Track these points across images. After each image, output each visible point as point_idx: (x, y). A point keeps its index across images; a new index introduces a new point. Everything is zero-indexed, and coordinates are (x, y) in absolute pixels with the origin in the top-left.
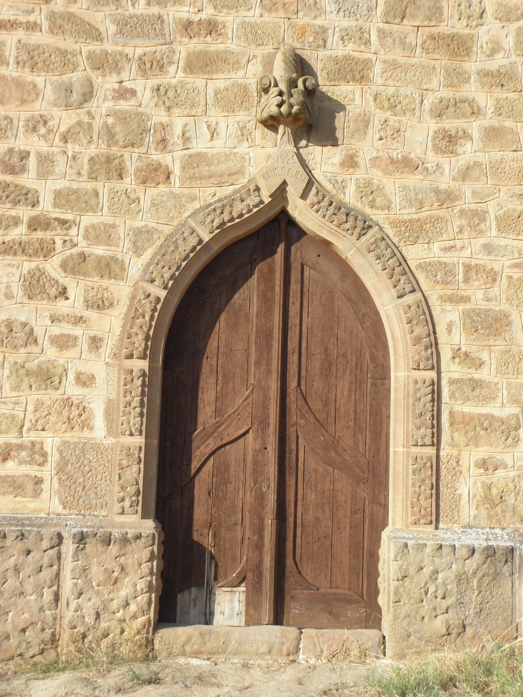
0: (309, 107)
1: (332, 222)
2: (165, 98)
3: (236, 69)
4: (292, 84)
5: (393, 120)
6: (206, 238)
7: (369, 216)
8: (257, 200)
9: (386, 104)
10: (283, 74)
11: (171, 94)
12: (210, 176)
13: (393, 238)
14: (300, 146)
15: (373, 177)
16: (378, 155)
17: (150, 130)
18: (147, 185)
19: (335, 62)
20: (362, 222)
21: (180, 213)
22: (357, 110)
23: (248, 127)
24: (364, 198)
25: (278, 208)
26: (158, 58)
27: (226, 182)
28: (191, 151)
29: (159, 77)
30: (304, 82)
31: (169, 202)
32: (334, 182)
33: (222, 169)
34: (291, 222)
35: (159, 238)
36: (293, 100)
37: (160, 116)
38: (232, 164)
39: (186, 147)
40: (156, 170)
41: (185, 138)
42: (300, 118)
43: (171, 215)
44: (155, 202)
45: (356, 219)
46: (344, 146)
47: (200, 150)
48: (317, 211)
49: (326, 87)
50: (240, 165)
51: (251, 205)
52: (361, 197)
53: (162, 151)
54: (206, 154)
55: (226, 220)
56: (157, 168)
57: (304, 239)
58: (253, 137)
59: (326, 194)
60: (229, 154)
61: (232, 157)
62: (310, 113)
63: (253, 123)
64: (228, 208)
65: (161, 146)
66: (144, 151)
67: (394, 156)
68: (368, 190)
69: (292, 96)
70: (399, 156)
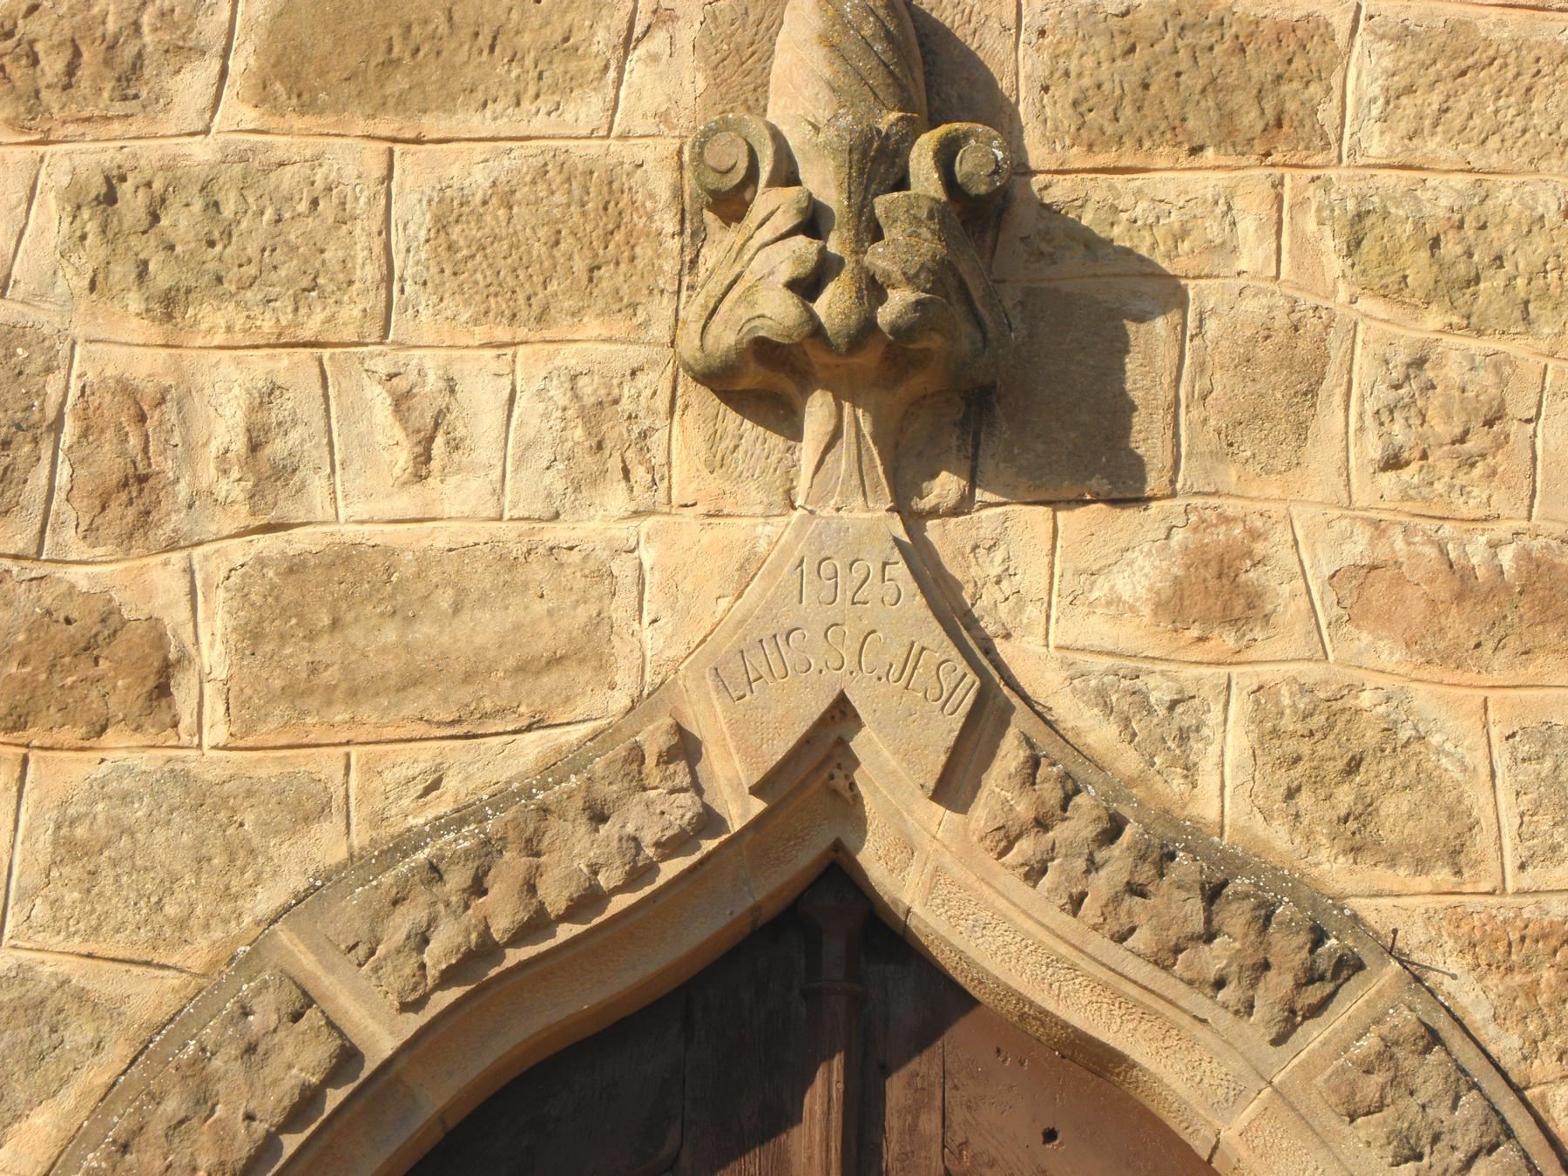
0: (976, 294)
1: (1121, 938)
2: (148, 248)
3: (554, 89)
4: (878, 166)
5: (1458, 357)
6: (382, 1036)
7: (1338, 901)
8: (682, 810)
9: (1418, 268)
10: (823, 115)
11: (181, 221)
12: (411, 681)
13: (1489, 1033)
14: (926, 503)
15: (1356, 676)
16: (1382, 552)
17: (57, 426)
18: (35, 735)
19: (1121, 43)
20: (1304, 938)
21: (227, 894)
22: (1252, 306)
23: (626, 405)
24: (1304, 800)
25: (806, 857)
26: (112, 26)
27: (500, 712)
28: (301, 540)
29: (117, 128)
30: (946, 156)
31: (160, 835)
32: (1124, 700)
33: (479, 640)
34: (884, 937)
35: (98, 1046)
36: (879, 258)
37: (117, 346)
38: (540, 607)
39: (271, 517)
40: (89, 648)
41: (266, 467)
42: (926, 354)
43: (171, 910)
44: (80, 832)
45: (1265, 917)
46: (1178, 503)
47: (351, 532)
48: (1034, 873)
49: (1066, 177)
50: (583, 614)
51: (648, 837)
52: (1291, 794)
53: (126, 540)
54: (389, 552)
55: (500, 928)
56: (96, 635)
57: (960, 1036)
58: (659, 458)
59: (1082, 771)
60: (517, 550)
61: (538, 571)
62: (979, 323)
63: (657, 380)
64: (512, 863)
65: (120, 514)
66: (21, 541)
67: (1477, 554)
68: (1327, 751)
69: (877, 234)
70: (1507, 556)
